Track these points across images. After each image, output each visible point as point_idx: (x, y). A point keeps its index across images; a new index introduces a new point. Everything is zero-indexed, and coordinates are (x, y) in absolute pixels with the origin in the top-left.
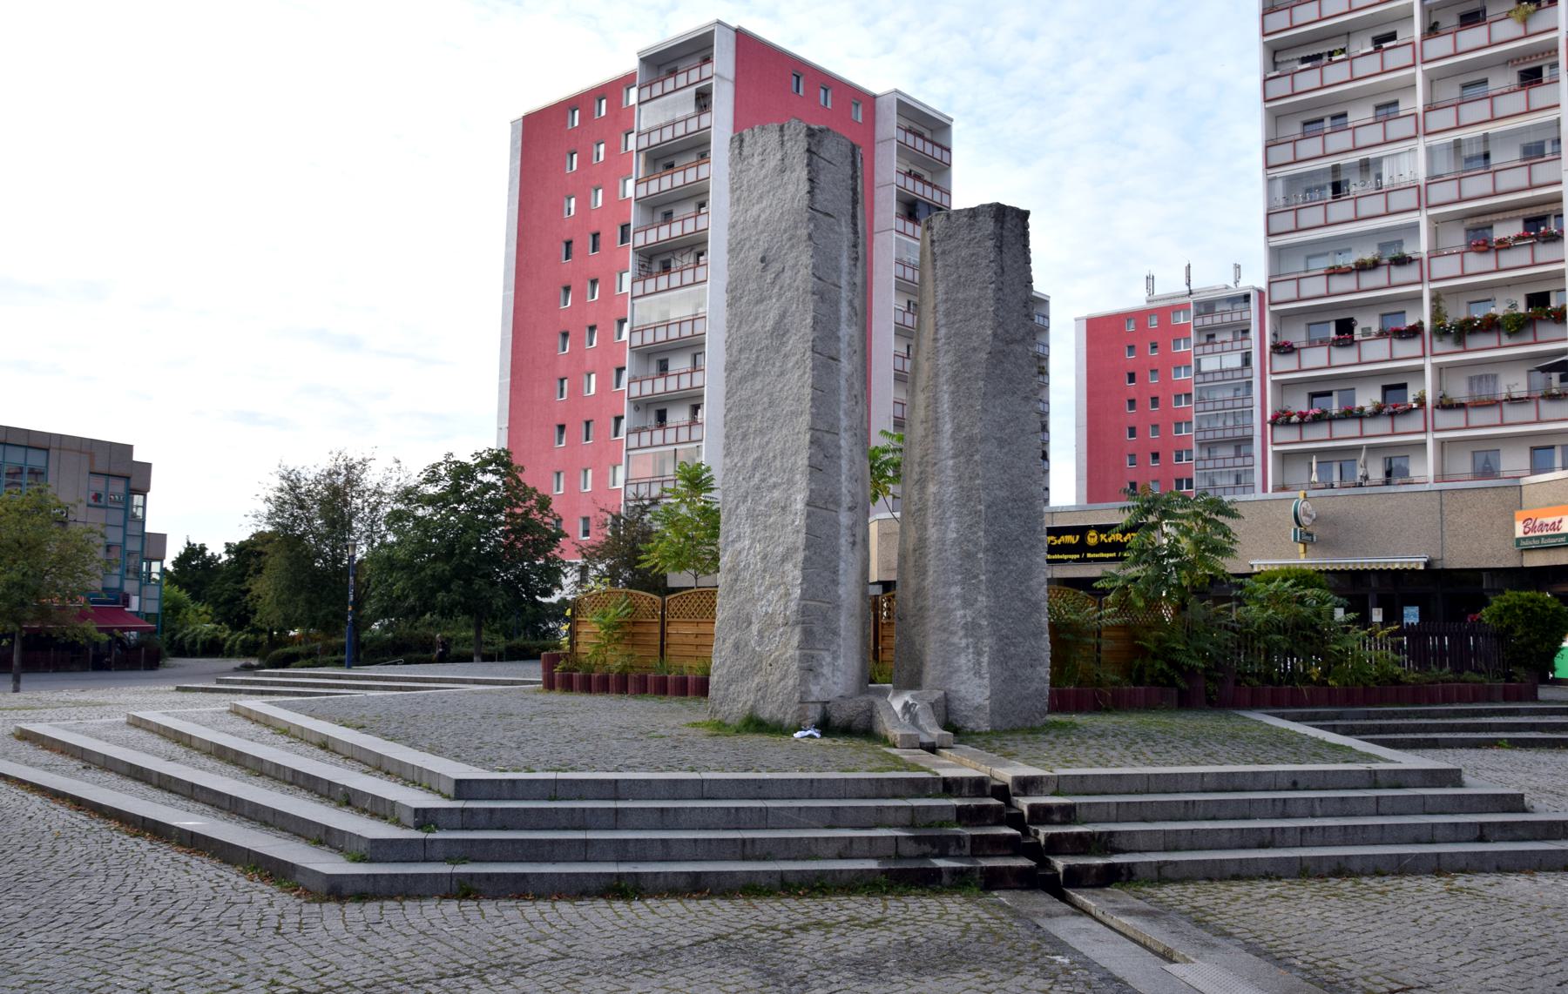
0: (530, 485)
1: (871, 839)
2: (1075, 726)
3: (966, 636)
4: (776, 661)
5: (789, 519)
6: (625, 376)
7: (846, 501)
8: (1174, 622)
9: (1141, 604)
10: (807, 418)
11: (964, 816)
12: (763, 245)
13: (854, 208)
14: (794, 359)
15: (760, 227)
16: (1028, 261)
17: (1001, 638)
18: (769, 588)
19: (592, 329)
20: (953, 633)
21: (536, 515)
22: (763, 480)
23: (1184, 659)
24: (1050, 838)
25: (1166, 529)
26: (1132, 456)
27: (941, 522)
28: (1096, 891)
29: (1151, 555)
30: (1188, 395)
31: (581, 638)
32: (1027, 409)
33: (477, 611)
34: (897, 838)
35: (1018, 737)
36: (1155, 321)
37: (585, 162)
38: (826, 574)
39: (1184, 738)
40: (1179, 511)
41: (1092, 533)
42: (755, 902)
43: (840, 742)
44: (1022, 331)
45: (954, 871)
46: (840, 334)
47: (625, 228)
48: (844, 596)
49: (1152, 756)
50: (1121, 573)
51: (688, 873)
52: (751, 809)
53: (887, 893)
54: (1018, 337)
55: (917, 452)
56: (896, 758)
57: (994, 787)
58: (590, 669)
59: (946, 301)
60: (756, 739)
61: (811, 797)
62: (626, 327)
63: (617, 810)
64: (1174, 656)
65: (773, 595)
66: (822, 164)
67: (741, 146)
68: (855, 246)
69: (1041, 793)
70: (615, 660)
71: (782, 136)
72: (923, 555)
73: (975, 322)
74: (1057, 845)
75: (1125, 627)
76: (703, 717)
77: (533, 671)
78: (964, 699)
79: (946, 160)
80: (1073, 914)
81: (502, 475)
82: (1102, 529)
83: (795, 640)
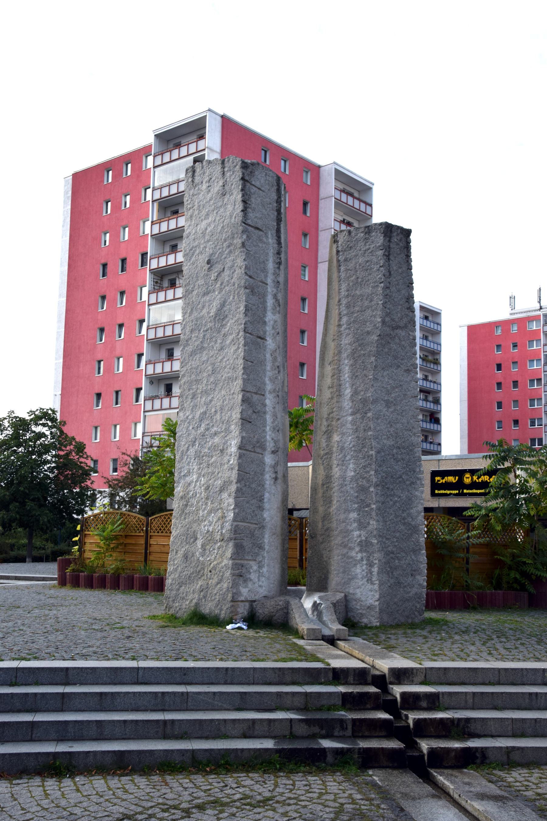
0: (70, 435)
1: (270, 721)
2: (446, 623)
3: (361, 551)
4: (214, 568)
5: (226, 459)
6: (144, 359)
7: (270, 446)
8: (524, 542)
9: (499, 528)
10: (240, 382)
11: (350, 701)
12: (209, 251)
13: (278, 225)
14: (231, 338)
15: (207, 237)
16: (410, 268)
17: (387, 553)
18: (210, 512)
19: (121, 326)
20: (351, 549)
21: (74, 456)
22: (207, 429)
23: (533, 571)
24: (418, 722)
25: (518, 472)
26: (500, 422)
27: (343, 463)
28: (455, 772)
29: (506, 490)
30: (539, 380)
31: (87, 547)
32: (409, 378)
33: (30, 524)
34: (291, 720)
35: (400, 631)
36: (515, 328)
37: (116, 208)
38: (254, 501)
39: (530, 635)
40: (527, 459)
41: (468, 475)
42: (168, 778)
43: (262, 633)
44: (405, 320)
45: (337, 752)
46: (267, 320)
47: (144, 255)
48: (268, 519)
49: (503, 651)
50: (484, 504)
51: (114, 752)
52: (174, 693)
53: (280, 770)
54: (401, 324)
55: (325, 411)
56: (301, 649)
57: (375, 677)
58: (93, 570)
59: (347, 296)
60: (195, 630)
61: (226, 683)
62: (145, 325)
63: (63, 695)
64: (524, 568)
65: (213, 518)
66: (253, 190)
67: (193, 176)
68: (279, 253)
69: (412, 683)
70: (111, 563)
71: (223, 168)
72: (329, 489)
73: (369, 312)
74: (423, 728)
75: (487, 545)
76: (160, 611)
77: (51, 570)
78: (359, 600)
79: (369, 212)
80: (433, 796)
81: (50, 428)
82: (473, 472)
83: (229, 553)
